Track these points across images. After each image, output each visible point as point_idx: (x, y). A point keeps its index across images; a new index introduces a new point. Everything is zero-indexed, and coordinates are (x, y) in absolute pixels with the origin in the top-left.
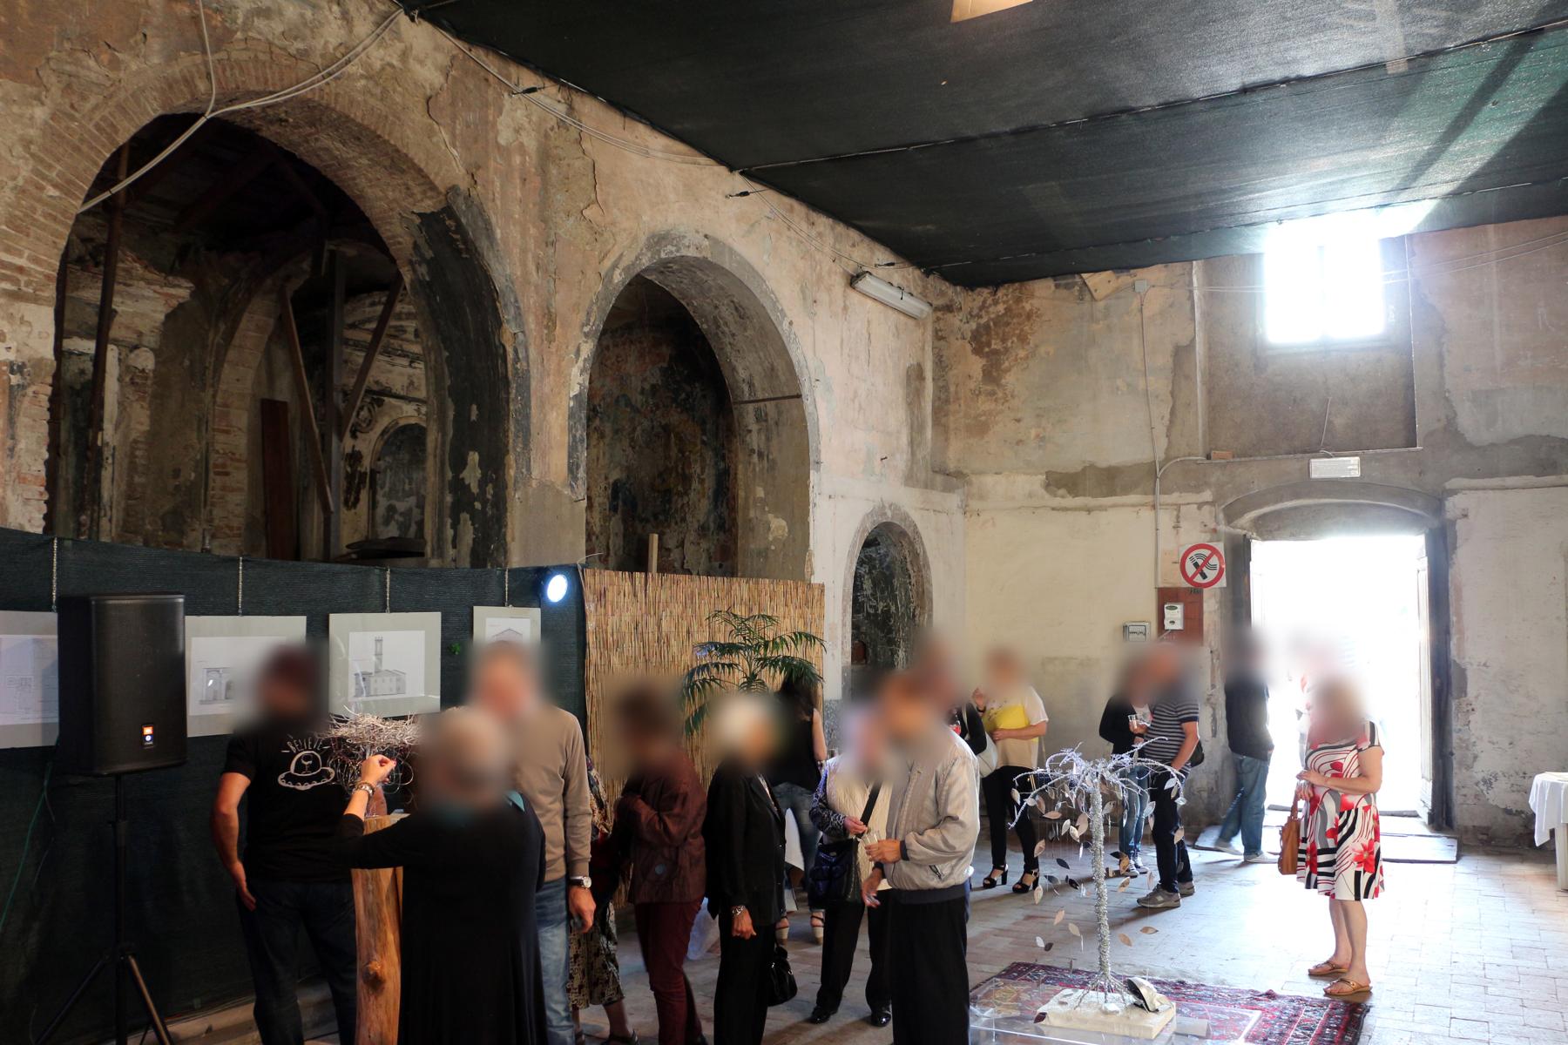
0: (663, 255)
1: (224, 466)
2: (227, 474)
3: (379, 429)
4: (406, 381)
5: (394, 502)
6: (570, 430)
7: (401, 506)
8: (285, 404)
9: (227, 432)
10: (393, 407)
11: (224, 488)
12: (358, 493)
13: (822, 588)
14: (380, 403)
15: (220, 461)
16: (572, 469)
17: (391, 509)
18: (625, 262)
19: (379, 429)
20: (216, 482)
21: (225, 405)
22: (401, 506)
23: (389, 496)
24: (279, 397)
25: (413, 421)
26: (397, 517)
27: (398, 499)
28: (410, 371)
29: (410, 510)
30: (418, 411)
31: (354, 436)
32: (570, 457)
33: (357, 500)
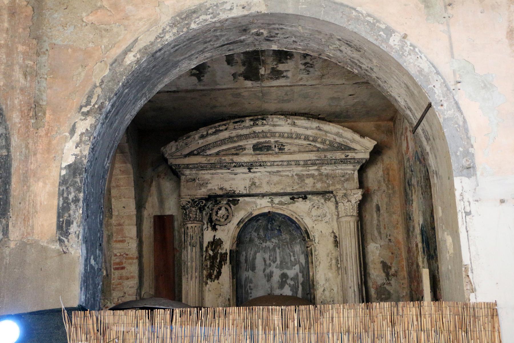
0: (193, 26)
1: (120, 263)
2: (123, 268)
3: (235, 221)
4: (248, 183)
5: (285, 271)
6: (61, 194)
7: (291, 273)
8: (171, 216)
9: (123, 241)
10: (247, 203)
11: (121, 278)
12: (220, 267)
13: (493, 311)
14: (235, 202)
15: (118, 260)
16: (63, 228)
17: (284, 276)
18: (141, 45)
19: (235, 221)
20: (116, 274)
21: (119, 225)
22: (291, 273)
23: (281, 267)
24: (168, 213)
25: (266, 210)
26: (289, 281)
27: (288, 268)
28: (251, 175)
29: (297, 275)
30: (272, 202)
31: (214, 229)
32: (59, 215)
33: (219, 273)
